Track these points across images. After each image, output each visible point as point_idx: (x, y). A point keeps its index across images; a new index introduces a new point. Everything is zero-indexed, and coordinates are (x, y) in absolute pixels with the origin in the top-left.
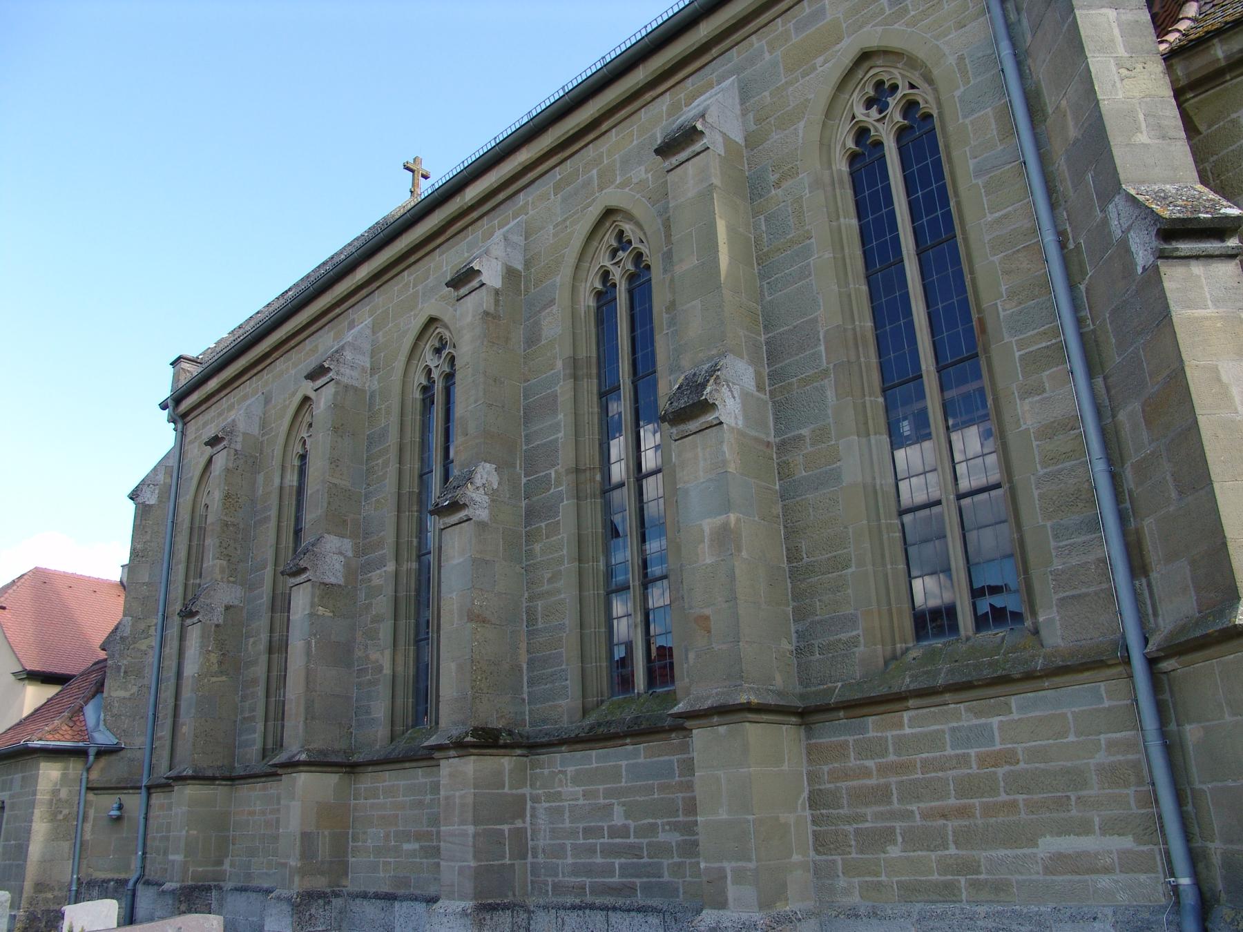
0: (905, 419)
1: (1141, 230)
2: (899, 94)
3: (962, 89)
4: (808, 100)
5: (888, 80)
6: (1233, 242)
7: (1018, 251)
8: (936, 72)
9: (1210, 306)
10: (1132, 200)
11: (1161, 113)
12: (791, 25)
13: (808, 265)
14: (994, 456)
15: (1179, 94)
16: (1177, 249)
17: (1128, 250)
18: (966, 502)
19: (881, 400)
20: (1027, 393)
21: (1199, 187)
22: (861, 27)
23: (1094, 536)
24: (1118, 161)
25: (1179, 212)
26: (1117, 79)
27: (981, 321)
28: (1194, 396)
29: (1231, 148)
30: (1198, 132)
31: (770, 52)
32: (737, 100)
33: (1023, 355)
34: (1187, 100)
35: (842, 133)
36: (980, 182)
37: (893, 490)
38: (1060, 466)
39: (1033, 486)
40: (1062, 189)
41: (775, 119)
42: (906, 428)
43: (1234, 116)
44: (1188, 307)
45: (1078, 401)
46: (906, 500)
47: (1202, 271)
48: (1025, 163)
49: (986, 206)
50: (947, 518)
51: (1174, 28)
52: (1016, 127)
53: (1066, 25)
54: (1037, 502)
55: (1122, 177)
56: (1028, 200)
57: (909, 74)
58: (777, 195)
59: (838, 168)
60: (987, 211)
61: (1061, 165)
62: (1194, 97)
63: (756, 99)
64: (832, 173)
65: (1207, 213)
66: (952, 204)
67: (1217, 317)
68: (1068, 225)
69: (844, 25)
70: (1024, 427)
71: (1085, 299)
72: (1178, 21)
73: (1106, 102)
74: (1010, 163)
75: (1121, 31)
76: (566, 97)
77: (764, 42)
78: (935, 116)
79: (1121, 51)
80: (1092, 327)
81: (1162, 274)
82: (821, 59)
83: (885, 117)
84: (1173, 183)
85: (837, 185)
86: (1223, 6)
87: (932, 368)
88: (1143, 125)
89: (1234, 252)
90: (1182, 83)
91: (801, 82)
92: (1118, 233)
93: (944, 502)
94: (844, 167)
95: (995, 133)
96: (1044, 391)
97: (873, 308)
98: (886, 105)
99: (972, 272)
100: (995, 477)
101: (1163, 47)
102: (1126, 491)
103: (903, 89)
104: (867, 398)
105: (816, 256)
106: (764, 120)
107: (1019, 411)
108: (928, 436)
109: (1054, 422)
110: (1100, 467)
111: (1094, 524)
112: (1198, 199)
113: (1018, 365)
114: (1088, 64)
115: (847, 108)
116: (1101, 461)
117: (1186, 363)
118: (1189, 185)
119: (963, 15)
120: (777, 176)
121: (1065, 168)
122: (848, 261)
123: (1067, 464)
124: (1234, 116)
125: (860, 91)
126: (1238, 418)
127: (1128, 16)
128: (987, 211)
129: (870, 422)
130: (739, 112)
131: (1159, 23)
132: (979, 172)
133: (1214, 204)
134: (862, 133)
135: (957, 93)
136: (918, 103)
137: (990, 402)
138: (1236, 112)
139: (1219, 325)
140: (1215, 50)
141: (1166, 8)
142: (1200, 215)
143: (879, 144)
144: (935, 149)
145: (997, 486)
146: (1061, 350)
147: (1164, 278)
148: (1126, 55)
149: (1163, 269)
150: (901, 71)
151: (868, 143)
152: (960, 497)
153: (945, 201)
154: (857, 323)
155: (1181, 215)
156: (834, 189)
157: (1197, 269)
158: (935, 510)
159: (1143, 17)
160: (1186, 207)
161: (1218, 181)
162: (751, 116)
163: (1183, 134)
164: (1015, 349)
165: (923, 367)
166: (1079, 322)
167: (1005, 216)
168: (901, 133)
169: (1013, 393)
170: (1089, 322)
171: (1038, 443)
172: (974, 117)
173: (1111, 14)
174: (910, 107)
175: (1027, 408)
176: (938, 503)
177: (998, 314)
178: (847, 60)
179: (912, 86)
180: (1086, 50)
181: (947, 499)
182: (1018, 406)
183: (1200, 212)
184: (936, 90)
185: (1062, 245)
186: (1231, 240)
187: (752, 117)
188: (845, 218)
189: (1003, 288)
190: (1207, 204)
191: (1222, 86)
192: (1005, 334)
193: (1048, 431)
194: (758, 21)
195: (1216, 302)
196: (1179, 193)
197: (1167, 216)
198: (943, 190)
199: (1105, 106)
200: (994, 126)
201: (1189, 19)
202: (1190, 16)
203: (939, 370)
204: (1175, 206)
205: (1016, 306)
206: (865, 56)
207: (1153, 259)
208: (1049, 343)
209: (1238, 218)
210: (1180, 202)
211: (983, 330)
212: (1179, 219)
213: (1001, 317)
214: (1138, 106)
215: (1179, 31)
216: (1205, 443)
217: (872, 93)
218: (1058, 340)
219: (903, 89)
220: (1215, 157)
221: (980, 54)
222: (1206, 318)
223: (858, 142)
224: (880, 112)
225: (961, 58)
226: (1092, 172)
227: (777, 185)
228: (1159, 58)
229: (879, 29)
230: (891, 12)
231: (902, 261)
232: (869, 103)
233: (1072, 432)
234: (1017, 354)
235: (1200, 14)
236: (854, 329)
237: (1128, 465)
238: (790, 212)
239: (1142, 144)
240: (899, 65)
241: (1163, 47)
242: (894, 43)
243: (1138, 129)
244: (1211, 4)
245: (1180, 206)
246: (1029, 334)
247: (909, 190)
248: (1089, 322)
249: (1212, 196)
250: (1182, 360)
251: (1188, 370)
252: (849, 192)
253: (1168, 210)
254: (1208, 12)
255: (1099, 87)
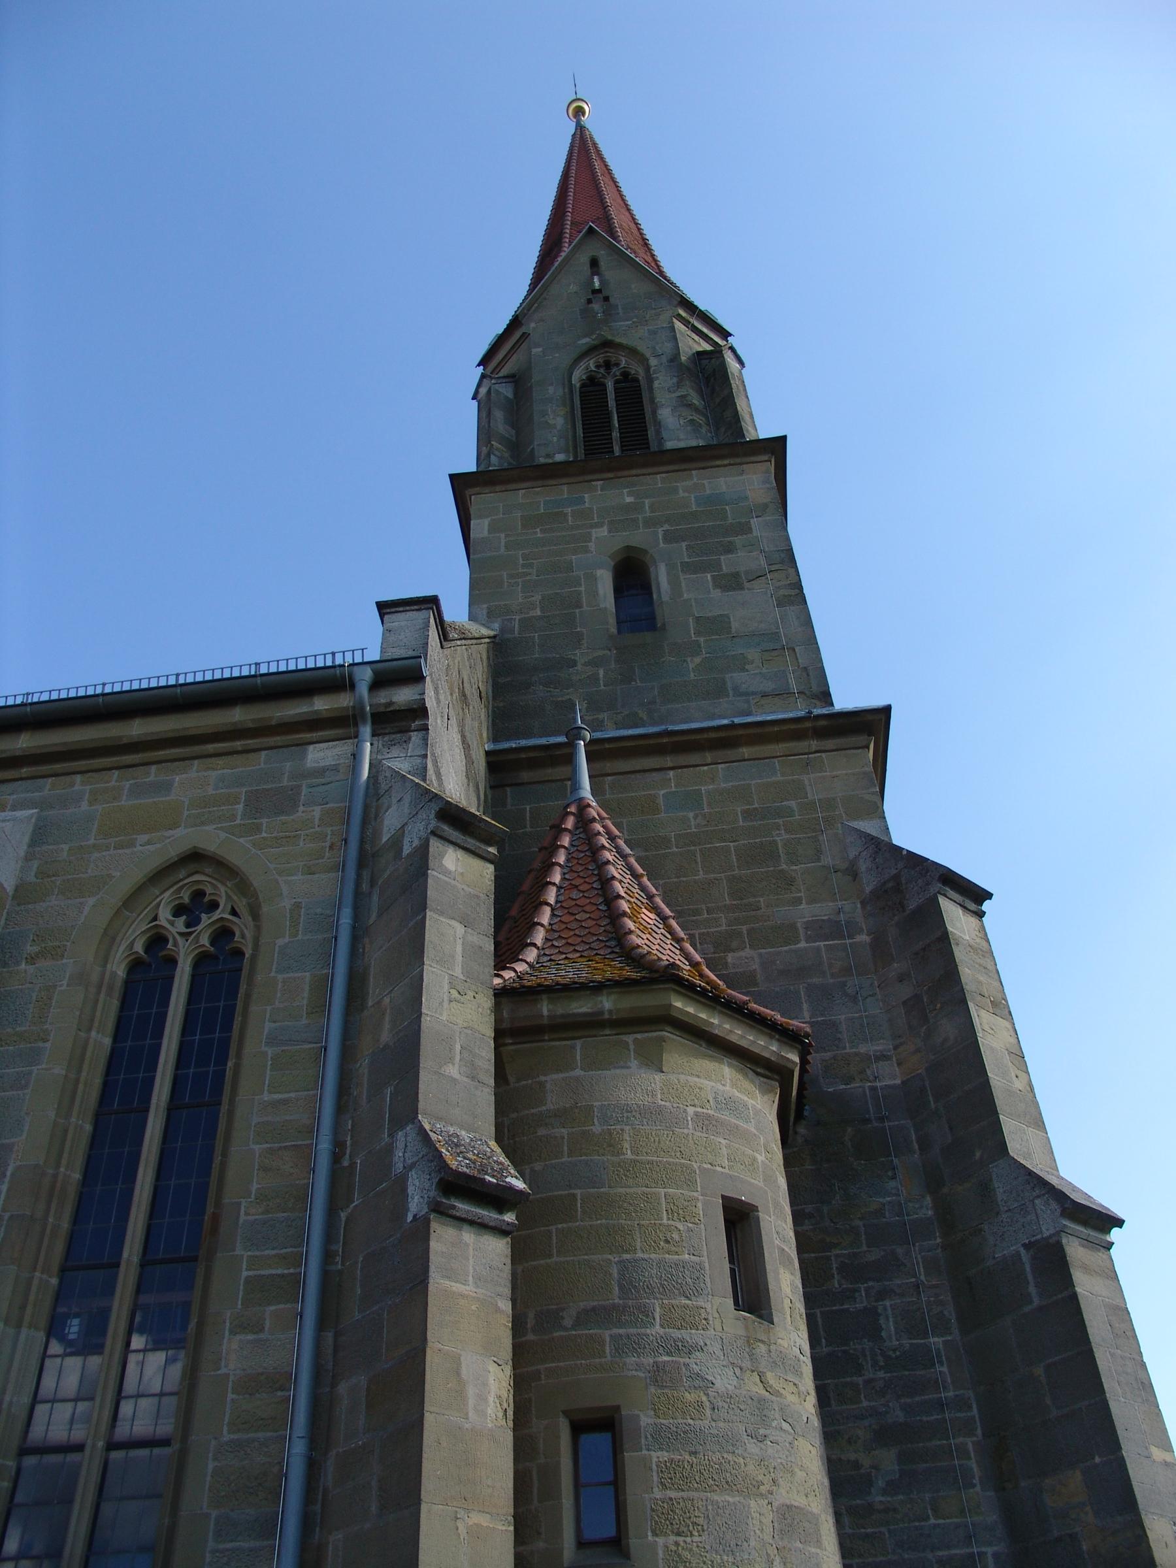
0: (77, 1315)
1: (423, 1172)
2: (216, 915)
3: (287, 940)
4: (110, 876)
5: (210, 894)
6: (510, 1217)
7: (285, 1147)
8: (265, 909)
9: (471, 1283)
10: (424, 1135)
11: (477, 1051)
12: (127, 784)
13: (30, 1073)
14: (173, 1400)
15: (500, 1035)
16: (454, 1207)
17: (404, 1190)
18: (116, 1455)
19: (54, 1281)
20: (241, 1327)
21: (493, 1144)
22: (203, 824)
23: (265, 1543)
24: (422, 1086)
25: (467, 1166)
26: (446, 999)
27: (216, 1218)
28: (427, 1387)
29: (533, 1111)
30: (507, 1082)
31: (91, 804)
32: (26, 839)
33: (250, 1276)
34: (506, 1045)
35: (134, 931)
36: (270, 1052)
37: (24, 1415)
38: (251, 1435)
39: (211, 1455)
40: (355, 1093)
41: (64, 881)
42: (74, 1328)
43: (542, 1078)
44: (449, 1278)
45: (298, 1354)
46: (37, 1432)
47: (472, 1240)
48: (325, 1050)
49: (267, 1082)
50: (83, 1472)
51: (512, 965)
52: (330, 1005)
53: (414, 921)
54: (209, 1478)
55: (421, 1105)
56: (315, 1092)
57: (235, 898)
58: (25, 971)
59: (114, 970)
60: (266, 1088)
61: (363, 1067)
62: (512, 1044)
63: (51, 847)
64: (103, 974)
65: (493, 1176)
66: (230, 1064)
67: (474, 1298)
68: (349, 1138)
69: (186, 813)
70: (223, 1371)
71: (342, 1232)
72: (517, 961)
73: (428, 1019)
74: (310, 1043)
75: (464, 950)
76: (101, 699)
77: (88, 788)
78: (247, 956)
79: (458, 972)
80: (340, 1267)
81: (432, 1231)
82: (145, 838)
83: (191, 933)
84: (468, 1131)
85: (104, 989)
86: (558, 964)
87: (136, 1259)
88: (458, 1058)
89: (508, 1228)
90: (504, 1026)
91: (112, 852)
92: (399, 1167)
93: (88, 1451)
94: (122, 973)
95: (305, 1002)
96: (262, 1330)
97: (89, 1157)
98: (197, 921)
99: (225, 1154)
100: (165, 1428)
101: (497, 981)
102: (321, 1488)
103: (223, 911)
104: (37, 1274)
105: (44, 1066)
106: (49, 876)
107: (224, 1347)
108: (98, 1349)
109: (262, 1374)
110: (299, 1448)
111: (268, 1527)
112: (489, 1158)
113: (241, 1287)
114: (422, 970)
115: (152, 906)
116: (303, 1440)
117: (430, 1344)
118: (484, 1138)
119: (317, 861)
120: (36, 949)
121: (366, 1071)
122: (81, 1087)
123: (260, 1435)
124: (542, 1078)
125: (172, 894)
126: (467, 1426)
127: (474, 939)
128: (266, 1088)
129: (29, 1310)
130: (22, 854)
131: (499, 954)
132: (272, 1040)
133: (500, 1172)
134: (157, 940)
135: (280, 942)
136: (233, 934)
137: (192, 1325)
138: (545, 1075)
139: (473, 1307)
140: (542, 1006)
141: (510, 940)
142: (486, 1177)
143: (172, 962)
144: (233, 992)
145: (165, 1442)
146: (292, 1287)
147: (433, 1236)
148: (461, 977)
149: (434, 1225)
150: (229, 892)
151: (160, 954)
152: (112, 1446)
153: (223, 1059)
154: (62, 1170)
155: (468, 1171)
156: (98, 993)
157: (468, 1236)
158: (72, 1457)
159: (487, 946)
160: (474, 1163)
161: (511, 1141)
162: (35, 864)
163: (492, 1082)
164: (244, 1267)
165: (125, 1255)
166: (328, 1256)
167: (285, 1102)
168: (202, 960)
169: (225, 1322)
170: (338, 1259)
171: (234, 1396)
172: (288, 975)
173: (460, 929)
174: (223, 934)
175: (235, 1346)
176: (79, 1448)
177: (238, 1218)
178: (173, 853)
179: (234, 912)
180: (425, 956)
181: (94, 1446)
182: (225, 1341)
183: (486, 1174)
184: (258, 928)
185: (336, 1158)
186: (509, 1214)
187: (36, 866)
188: (98, 1032)
189: (255, 1187)
190: (496, 1167)
191: (539, 1044)
192: (238, 1244)
193: (250, 1384)
194: (92, 762)
195: (478, 1279)
196: (472, 1144)
197: (454, 1167)
198: (225, 1045)
199: (426, 1021)
200: (306, 995)
201: (527, 963)
202: (528, 960)
203: (143, 1265)
204: (465, 1158)
205: (262, 1213)
206: (195, 858)
207: (427, 1210)
208: (286, 1272)
209: (521, 1192)
210: (470, 1155)
211: (215, 1230)
212: (464, 1174)
213: (241, 1221)
214: (458, 1034)
215: (515, 971)
216: (425, 1449)
217: (186, 900)
218: (298, 1270)
219: (223, 911)
220: (514, 1115)
221: (319, 911)
222: (462, 1296)
223: (148, 948)
224: (188, 925)
225: (298, 906)
226: (392, 1088)
227: (31, 960)
228: (491, 992)
229: (223, 835)
230: (242, 822)
231: (147, 1110)
232: (178, 911)
233: (279, 1393)
234: (245, 1274)
235: (537, 963)
236: (55, 1176)
237: (333, 1453)
238: (34, 998)
239: (451, 1077)
240: (229, 885)
241: (497, 981)
242: (234, 858)
243: (451, 1060)
244: (549, 958)
245: (470, 1160)
246: (267, 1252)
247: (186, 1029)
248: (338, 1259)
249: (502, 1158)
250: (426, 1339)
251: (429, 1352)
252: (115, 1003)
253: (457, 1160)
254: (544, 964)
255: (426, 1000)
